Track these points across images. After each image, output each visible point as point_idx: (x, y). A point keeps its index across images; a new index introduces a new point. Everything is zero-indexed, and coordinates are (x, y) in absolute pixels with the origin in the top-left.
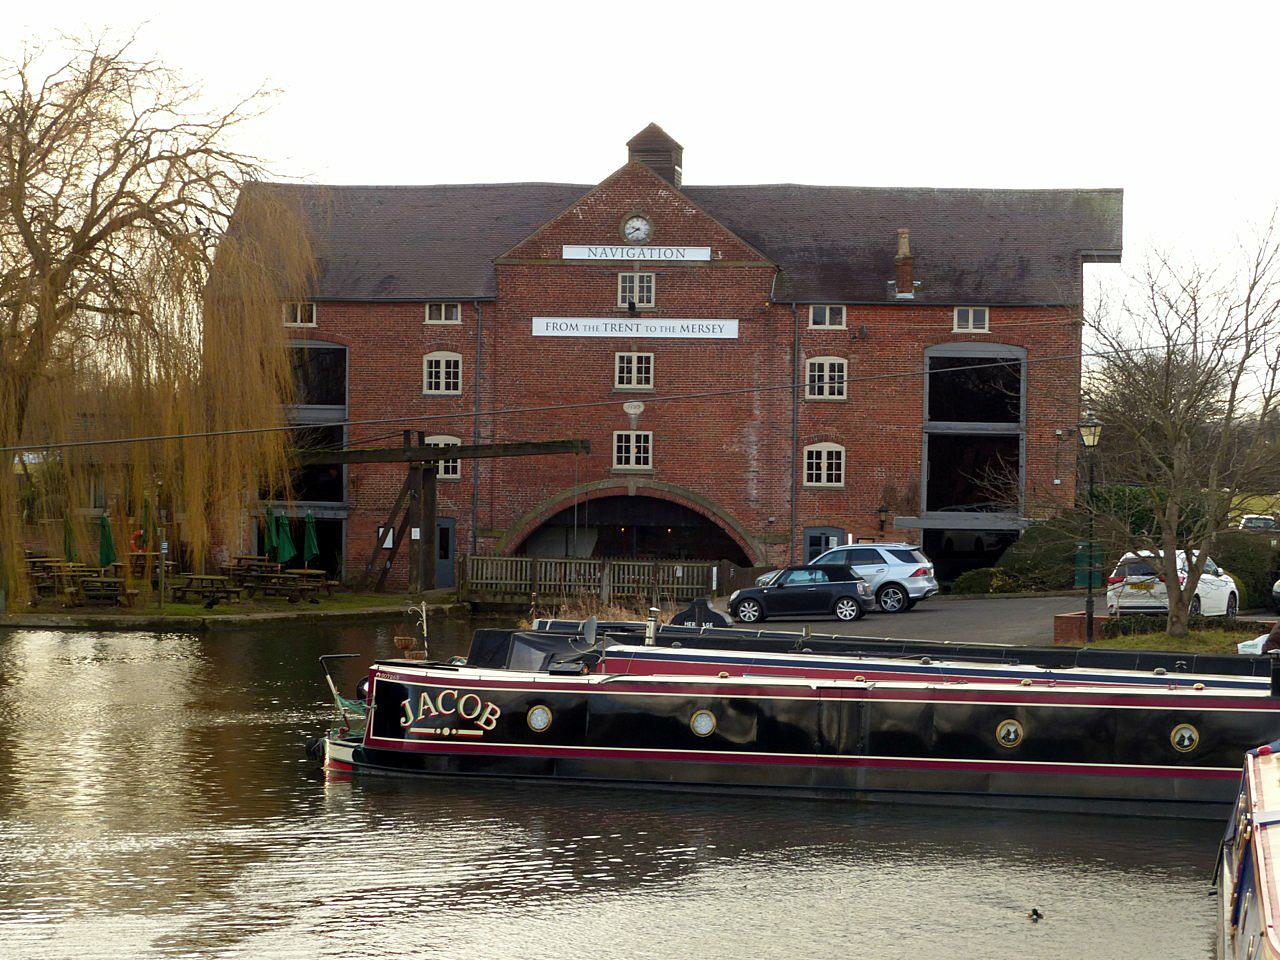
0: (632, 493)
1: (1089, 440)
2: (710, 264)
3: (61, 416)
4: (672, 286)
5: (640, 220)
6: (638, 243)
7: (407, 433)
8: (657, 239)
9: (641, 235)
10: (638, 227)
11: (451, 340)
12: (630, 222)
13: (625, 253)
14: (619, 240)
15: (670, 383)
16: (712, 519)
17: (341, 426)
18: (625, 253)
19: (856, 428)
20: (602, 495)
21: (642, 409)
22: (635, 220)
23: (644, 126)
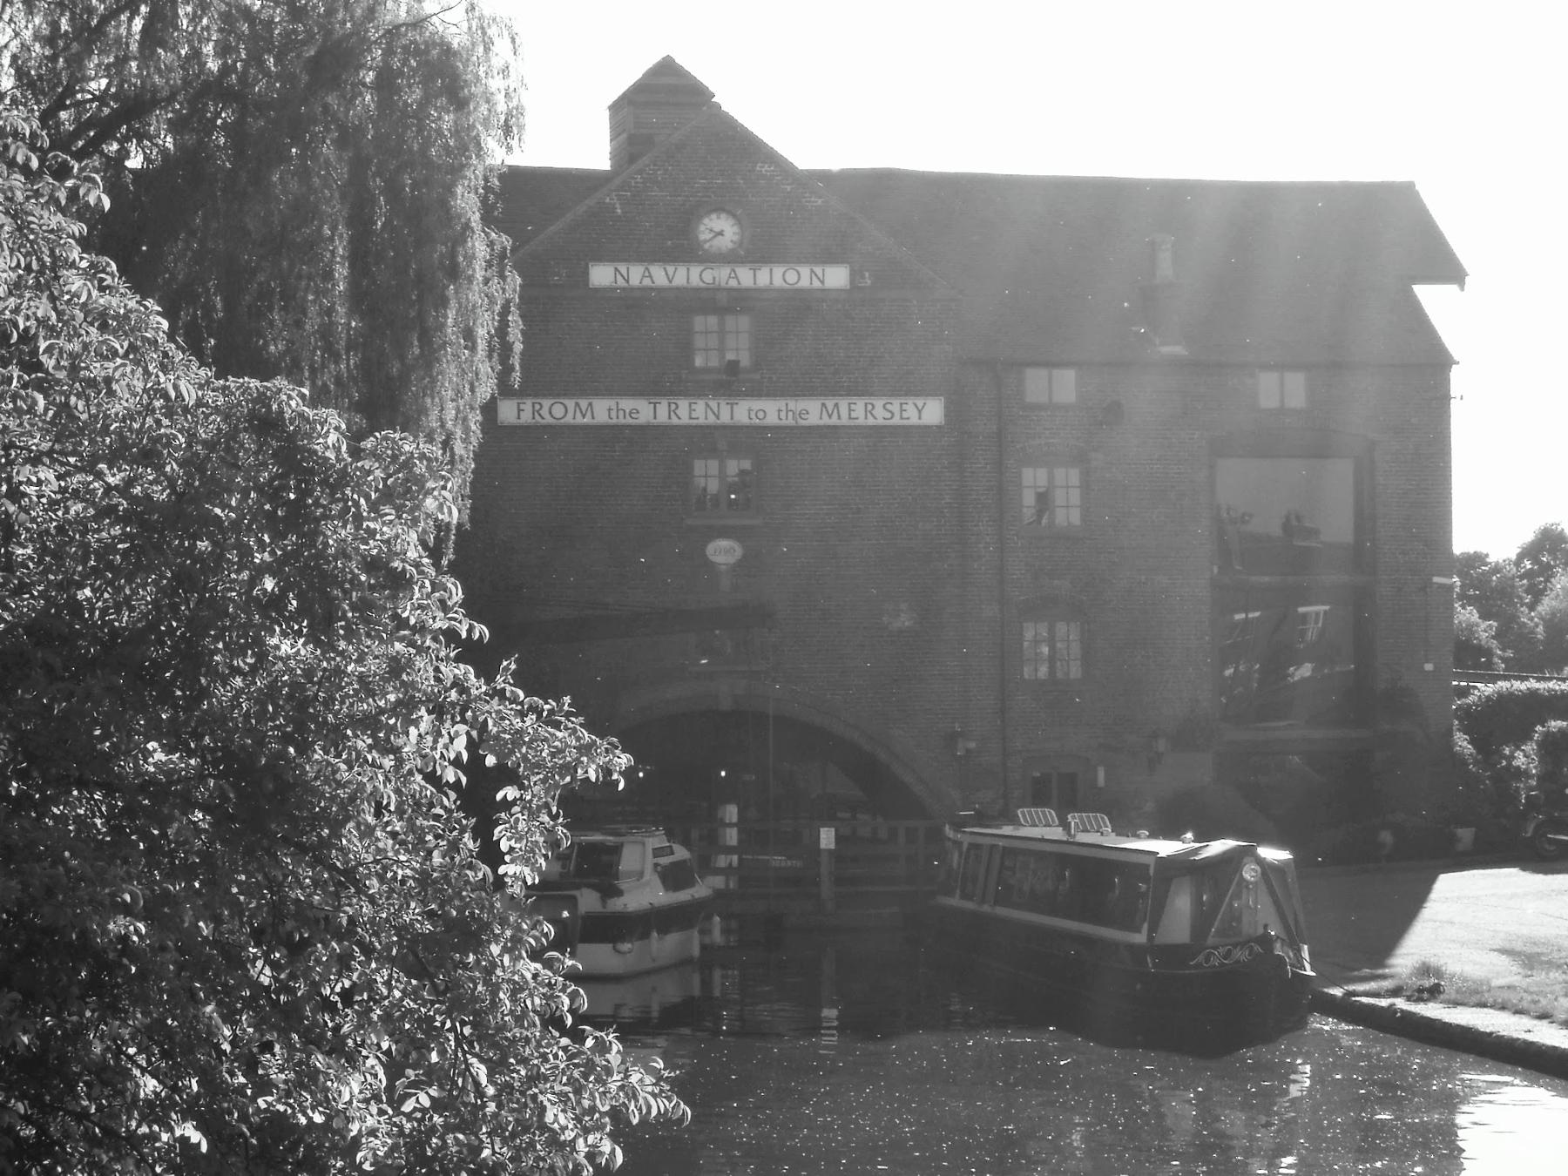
14: (685, 250)
18: (544, 412)
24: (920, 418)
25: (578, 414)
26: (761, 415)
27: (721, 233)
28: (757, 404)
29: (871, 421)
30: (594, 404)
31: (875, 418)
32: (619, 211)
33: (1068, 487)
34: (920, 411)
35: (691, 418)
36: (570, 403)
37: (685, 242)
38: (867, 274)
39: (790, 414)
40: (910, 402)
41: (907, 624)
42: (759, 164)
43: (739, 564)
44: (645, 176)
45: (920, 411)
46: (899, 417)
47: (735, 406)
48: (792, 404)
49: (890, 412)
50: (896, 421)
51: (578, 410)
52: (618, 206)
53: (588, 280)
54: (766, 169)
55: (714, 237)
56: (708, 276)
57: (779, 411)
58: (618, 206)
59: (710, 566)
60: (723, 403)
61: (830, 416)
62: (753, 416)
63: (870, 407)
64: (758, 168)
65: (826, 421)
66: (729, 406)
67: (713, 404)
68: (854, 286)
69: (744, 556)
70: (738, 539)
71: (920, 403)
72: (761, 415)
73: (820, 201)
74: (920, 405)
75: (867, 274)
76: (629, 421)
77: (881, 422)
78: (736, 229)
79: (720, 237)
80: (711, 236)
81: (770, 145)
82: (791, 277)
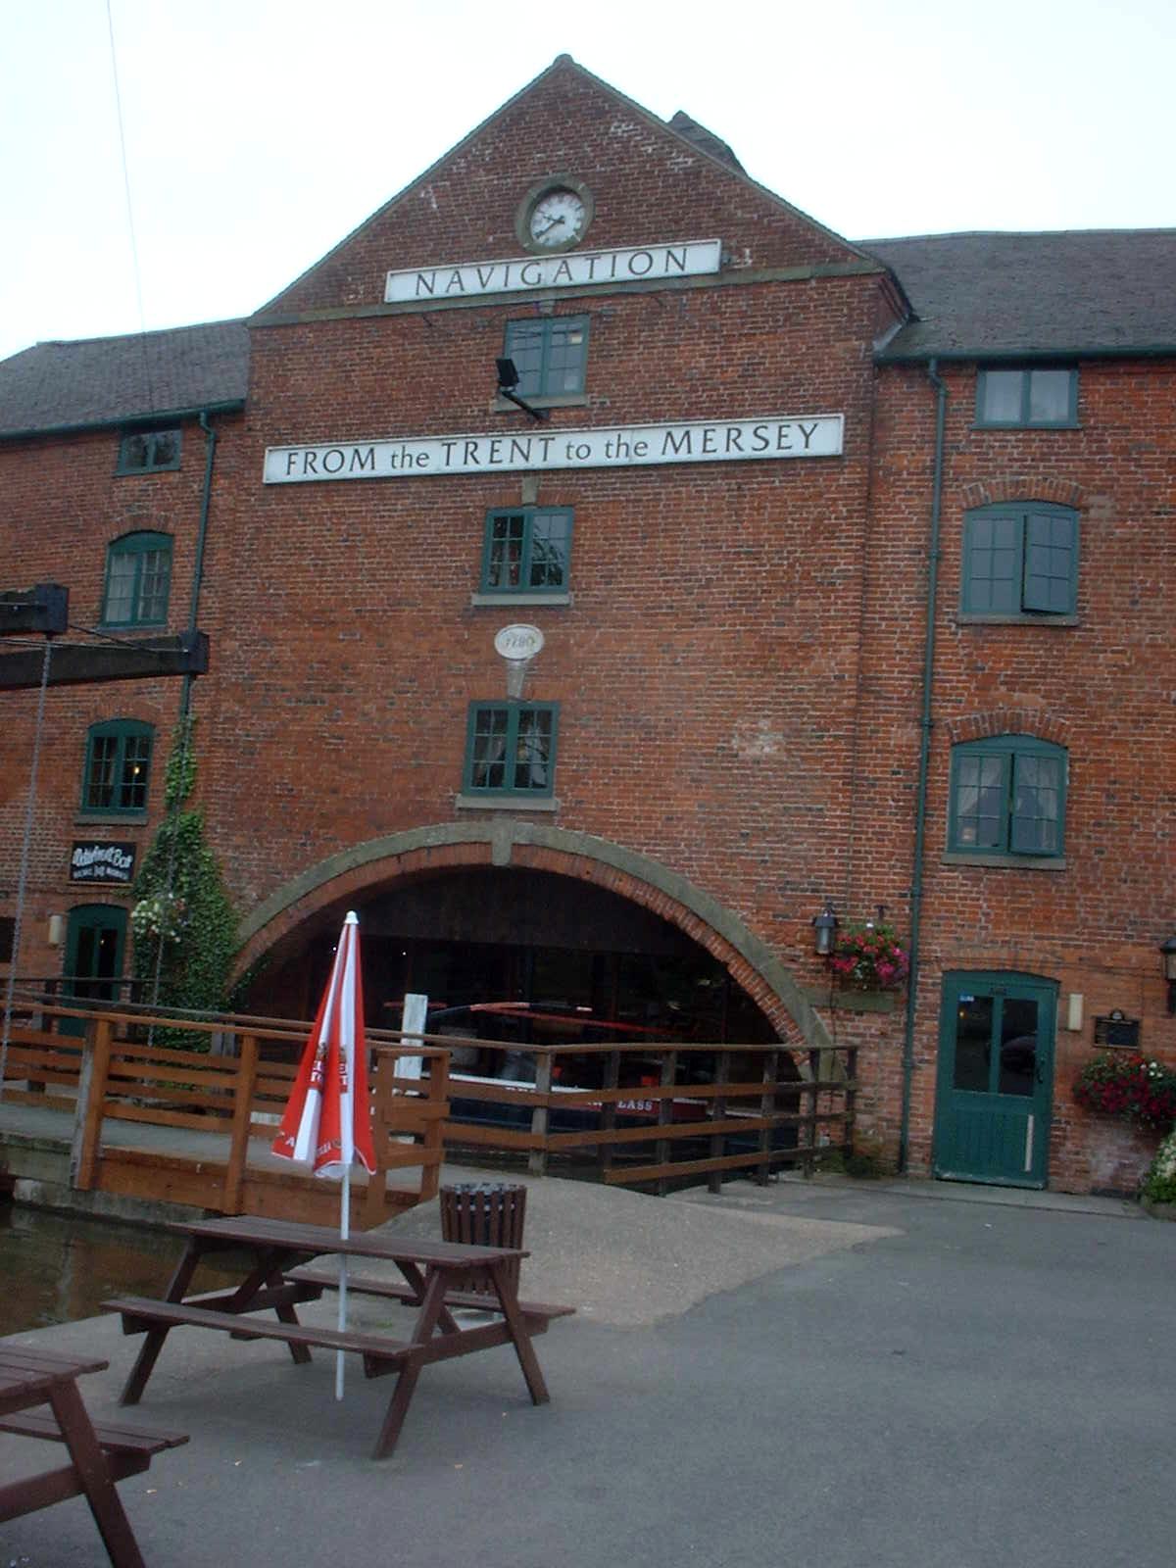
0: (501, 858)
1: (766, 746)
2: (721, 282)
3: (1067, 936)
4: (627, 343)
5: (567, 198)
6: (571, 247)
7: (591, 352)
8: (593, 239)
9: (568, 231)
10: (564, 217)
11: (159, 507)
12: (544, 207)
13: (318, 464)
14: (518, 247)
15: (609, 579)
16: (697, 934)
17: (208, 1034)
18: (318, 464)
19: (1101, 696)
20: (433, 861)
21: (537, 647)
22: (555, 200)
23: (546, 62)
24: (807, 446)
25: (357, 465)
26: (583, 452)
27: (561, 221)
28: (579, 439)
29: (734, 454)
30: (375, 451)
31: (740, 449)
32: (435, 206)
33: (991, 580)
34: (807, 436)
35: (492, 461)
36: (348, 452)
37: (511, 235)
38: (747, 251)
39: (623, 449)
40: (794, 426)
41: (767, 750)
42: (616, 124)
43: (538, 658)
44: (470, 158)
45: (807, 436)
46: (776, 445)
47: (452, 447)
48: (626, 437)
49: (760, 437)
50: (772, 451)
51: (356, 459)
52: (433, 200)
53: (383, 292)
54: (620, 129)
55: (552, 226)
56: (532, 275)
57: (608, 445)
58: (433, 200)
59: (500, 661)
60: (535, 440)
61: (677, 450)
62: (573, 451)
63: (734, 434)
64: (612, 129)
65: (670, 456)
66: (543, 442)
67: (522, 442)
68: (725, 267)
69: (545, 649)
70: (542, 626)
71: (808, 426)
72: (583, 452)
73: (690, 160)
74: (808, 429)
75: (747, 251)
76: (416, 470)
77: (748, 453)
78: (581, 213)
79: (562, 226)
80: (548, 225)
81: (834, 230)
82: (641, 263)
